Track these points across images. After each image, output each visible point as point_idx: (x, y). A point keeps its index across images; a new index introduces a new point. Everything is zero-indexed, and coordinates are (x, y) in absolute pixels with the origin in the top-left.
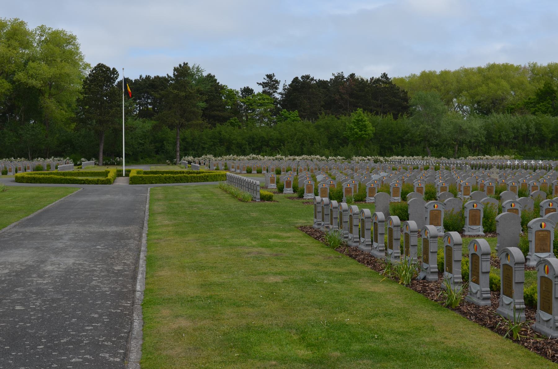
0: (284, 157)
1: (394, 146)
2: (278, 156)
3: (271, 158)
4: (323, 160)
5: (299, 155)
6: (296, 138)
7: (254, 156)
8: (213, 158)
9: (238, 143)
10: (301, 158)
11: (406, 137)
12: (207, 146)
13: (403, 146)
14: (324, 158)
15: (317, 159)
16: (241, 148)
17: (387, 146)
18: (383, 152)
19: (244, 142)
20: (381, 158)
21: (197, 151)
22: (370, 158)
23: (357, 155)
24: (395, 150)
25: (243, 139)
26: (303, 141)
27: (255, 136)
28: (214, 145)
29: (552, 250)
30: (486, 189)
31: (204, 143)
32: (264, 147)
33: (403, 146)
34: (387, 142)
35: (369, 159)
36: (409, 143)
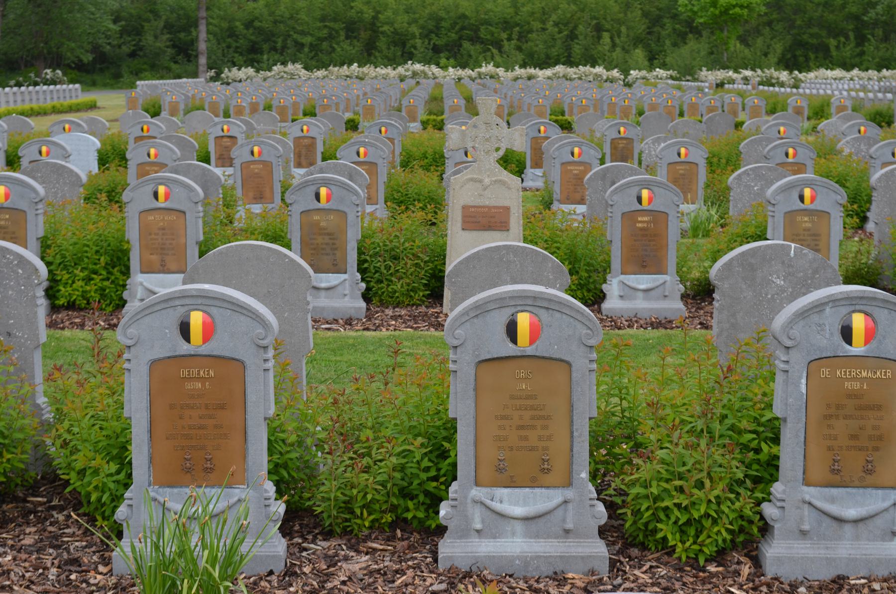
0: (501, 71)
1: (833, 42)
2: (488, 68)
3: (468, 72)
4: (611, 80)
5: (542, 65)
6: (554, 17)
7: (418, 67)
8: (303, 72)
9: (395, 32)
10: (548, 72)
11: (872, 14)
12: (307, 40)
13: (861, 40)
14: (615, 73)
15: (597, 76)
16: (404, 44)
17: (814, 41)
18: (801, 59)
19: (415, 29)
20: (784, 76)
21: (282, 54)
22: (748, 73)
23: (716, 63)
24: (834, 53)
25: (415, 21)
26: (575, 27)
27: (443, 14)
28: (330, 37)
29: (701, 193)
30: (617, 110)
31: (303, 33)
32: (466, 45)
33: (861, 40)
34: (815, 30)
35: (746, 80)
36: (879, 32)
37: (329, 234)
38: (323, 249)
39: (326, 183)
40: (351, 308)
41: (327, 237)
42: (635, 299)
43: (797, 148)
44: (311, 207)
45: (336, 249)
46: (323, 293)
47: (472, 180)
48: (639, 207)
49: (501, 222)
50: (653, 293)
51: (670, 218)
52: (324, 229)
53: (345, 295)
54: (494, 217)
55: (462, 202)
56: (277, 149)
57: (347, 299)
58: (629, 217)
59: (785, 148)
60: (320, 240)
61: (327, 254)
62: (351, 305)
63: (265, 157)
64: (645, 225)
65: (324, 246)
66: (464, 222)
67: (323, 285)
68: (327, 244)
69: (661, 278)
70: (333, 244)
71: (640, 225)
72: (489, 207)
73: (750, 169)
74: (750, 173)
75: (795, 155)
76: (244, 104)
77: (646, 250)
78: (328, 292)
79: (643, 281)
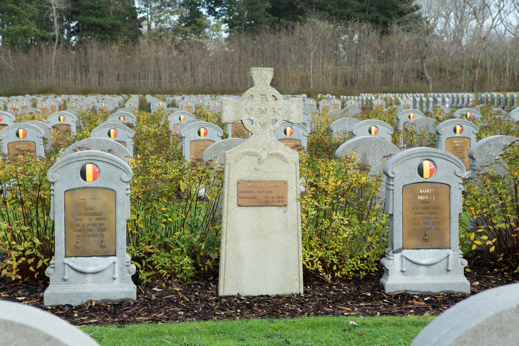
37: (95, 214)
38: (90, 230)
39: (93, 160)
40: (121, 293)
41: (93, 218)
42: (417, 275)
43: (463, 125)
44: (76, 186)
45: (104, 230)
46: (90, 278)
47: (248, 154)
48: (421, 179)
49: (279, 197)
50: (435, 267)
51: (452, 190)
52: (91, 209)
53: (114, 279)
54: (271, 192)
55: (238, 178)
56: (39, 131)
57: (116, 282)
58: (409, 189)
59: (454, 126)
60: (86, 220)
61: (94, 236)
62: (121, 290)
63: (28, 138)
64: (427, 197)
65: (91, 227)
66: (239, 197)
67: (90, 269)
68: (94, 225)
69: (443, 253)
70: (101, 224)
71: (421, 198)
72: (265, 182)
73: (492, 140)
74: (492, 143)
75: (461, 131)
76: (17, 107)
77: (427, 223)
78: (96, 276)
79: (426, 256)
